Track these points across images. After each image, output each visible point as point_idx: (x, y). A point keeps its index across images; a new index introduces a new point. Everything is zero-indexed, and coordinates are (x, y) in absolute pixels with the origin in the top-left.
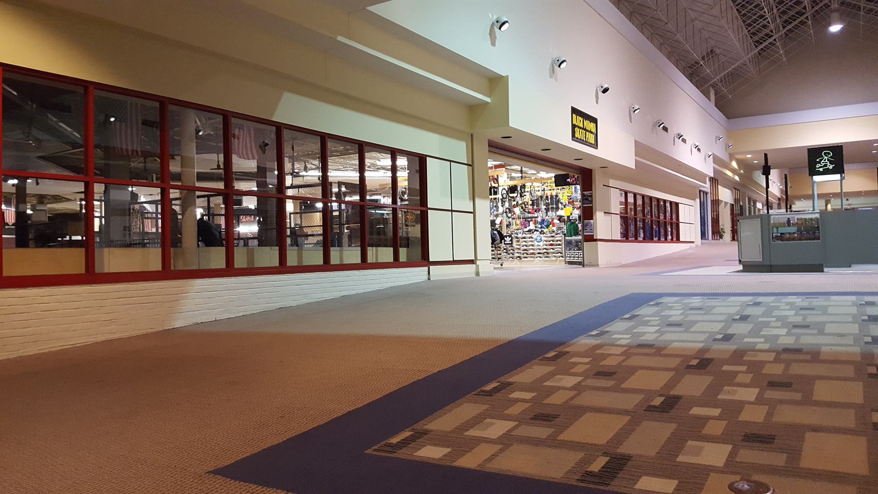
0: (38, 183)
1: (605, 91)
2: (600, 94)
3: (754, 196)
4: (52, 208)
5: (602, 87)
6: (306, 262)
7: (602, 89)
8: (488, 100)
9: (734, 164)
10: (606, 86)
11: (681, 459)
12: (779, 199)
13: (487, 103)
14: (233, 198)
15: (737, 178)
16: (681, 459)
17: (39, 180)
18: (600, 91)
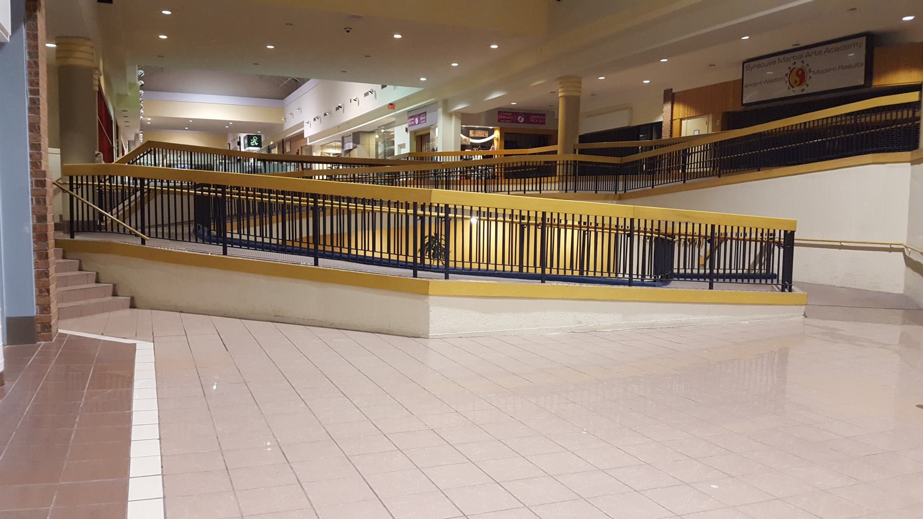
17: (419, 272)
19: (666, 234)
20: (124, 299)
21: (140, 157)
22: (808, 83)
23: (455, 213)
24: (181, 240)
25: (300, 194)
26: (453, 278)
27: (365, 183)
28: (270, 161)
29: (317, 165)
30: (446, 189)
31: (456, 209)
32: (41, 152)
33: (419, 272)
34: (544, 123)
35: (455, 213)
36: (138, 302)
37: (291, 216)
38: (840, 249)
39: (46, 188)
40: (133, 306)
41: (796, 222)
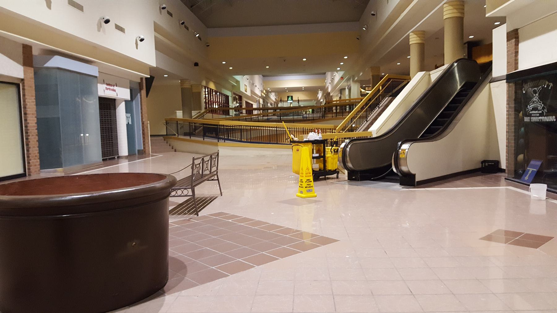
0: (225, 142)
1: (142, 40)
2: (139, 42)
3: (268, 101)
4: (27, 198)
5: (140, 37)
6: (271, 143)
7: (140, 39)
8: (235, 84)
9: (264, 92)
10: (142, 37)
11: (487, 16)
12: (275, 102)
13: (236, 85)
14: (553, 84)
15: (264, 96)
16: (487, 16)
17: (226, 141)
18: (138, 39)
19: (275, 119)
20: (174, 150)
21: (205, 115)
22: (336, 156)
23: (292, 129)
24: (276, 142)
25: (242, 126)
26: (227, 142)
27: (113, 86)
28: (265, 110)
29: (270, 110)
30: (349, 132)
31: (299, 128)
32: (27, 103)
33: (226, 141)
34: (307, 190)
35: (292, 129)
36: (177, 150)
37: (260, 134)
38: (138, 45)
39: (28, 128)
40: (175, 151)
41: (415, 174)
